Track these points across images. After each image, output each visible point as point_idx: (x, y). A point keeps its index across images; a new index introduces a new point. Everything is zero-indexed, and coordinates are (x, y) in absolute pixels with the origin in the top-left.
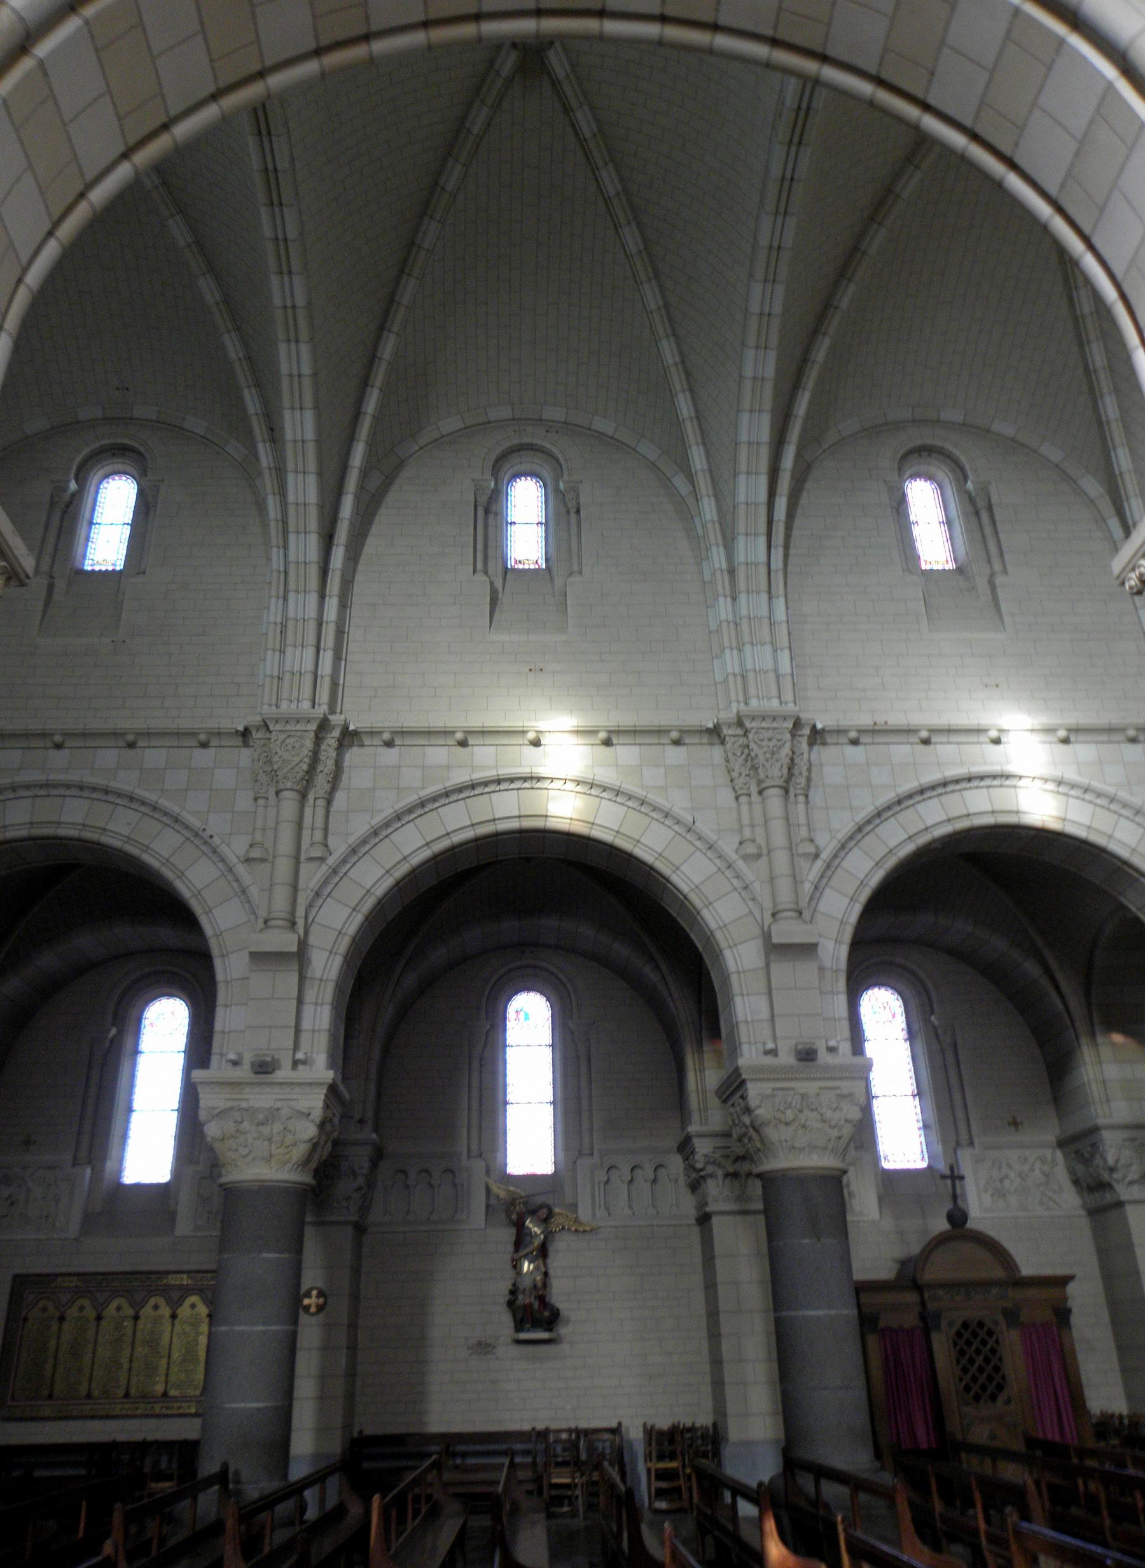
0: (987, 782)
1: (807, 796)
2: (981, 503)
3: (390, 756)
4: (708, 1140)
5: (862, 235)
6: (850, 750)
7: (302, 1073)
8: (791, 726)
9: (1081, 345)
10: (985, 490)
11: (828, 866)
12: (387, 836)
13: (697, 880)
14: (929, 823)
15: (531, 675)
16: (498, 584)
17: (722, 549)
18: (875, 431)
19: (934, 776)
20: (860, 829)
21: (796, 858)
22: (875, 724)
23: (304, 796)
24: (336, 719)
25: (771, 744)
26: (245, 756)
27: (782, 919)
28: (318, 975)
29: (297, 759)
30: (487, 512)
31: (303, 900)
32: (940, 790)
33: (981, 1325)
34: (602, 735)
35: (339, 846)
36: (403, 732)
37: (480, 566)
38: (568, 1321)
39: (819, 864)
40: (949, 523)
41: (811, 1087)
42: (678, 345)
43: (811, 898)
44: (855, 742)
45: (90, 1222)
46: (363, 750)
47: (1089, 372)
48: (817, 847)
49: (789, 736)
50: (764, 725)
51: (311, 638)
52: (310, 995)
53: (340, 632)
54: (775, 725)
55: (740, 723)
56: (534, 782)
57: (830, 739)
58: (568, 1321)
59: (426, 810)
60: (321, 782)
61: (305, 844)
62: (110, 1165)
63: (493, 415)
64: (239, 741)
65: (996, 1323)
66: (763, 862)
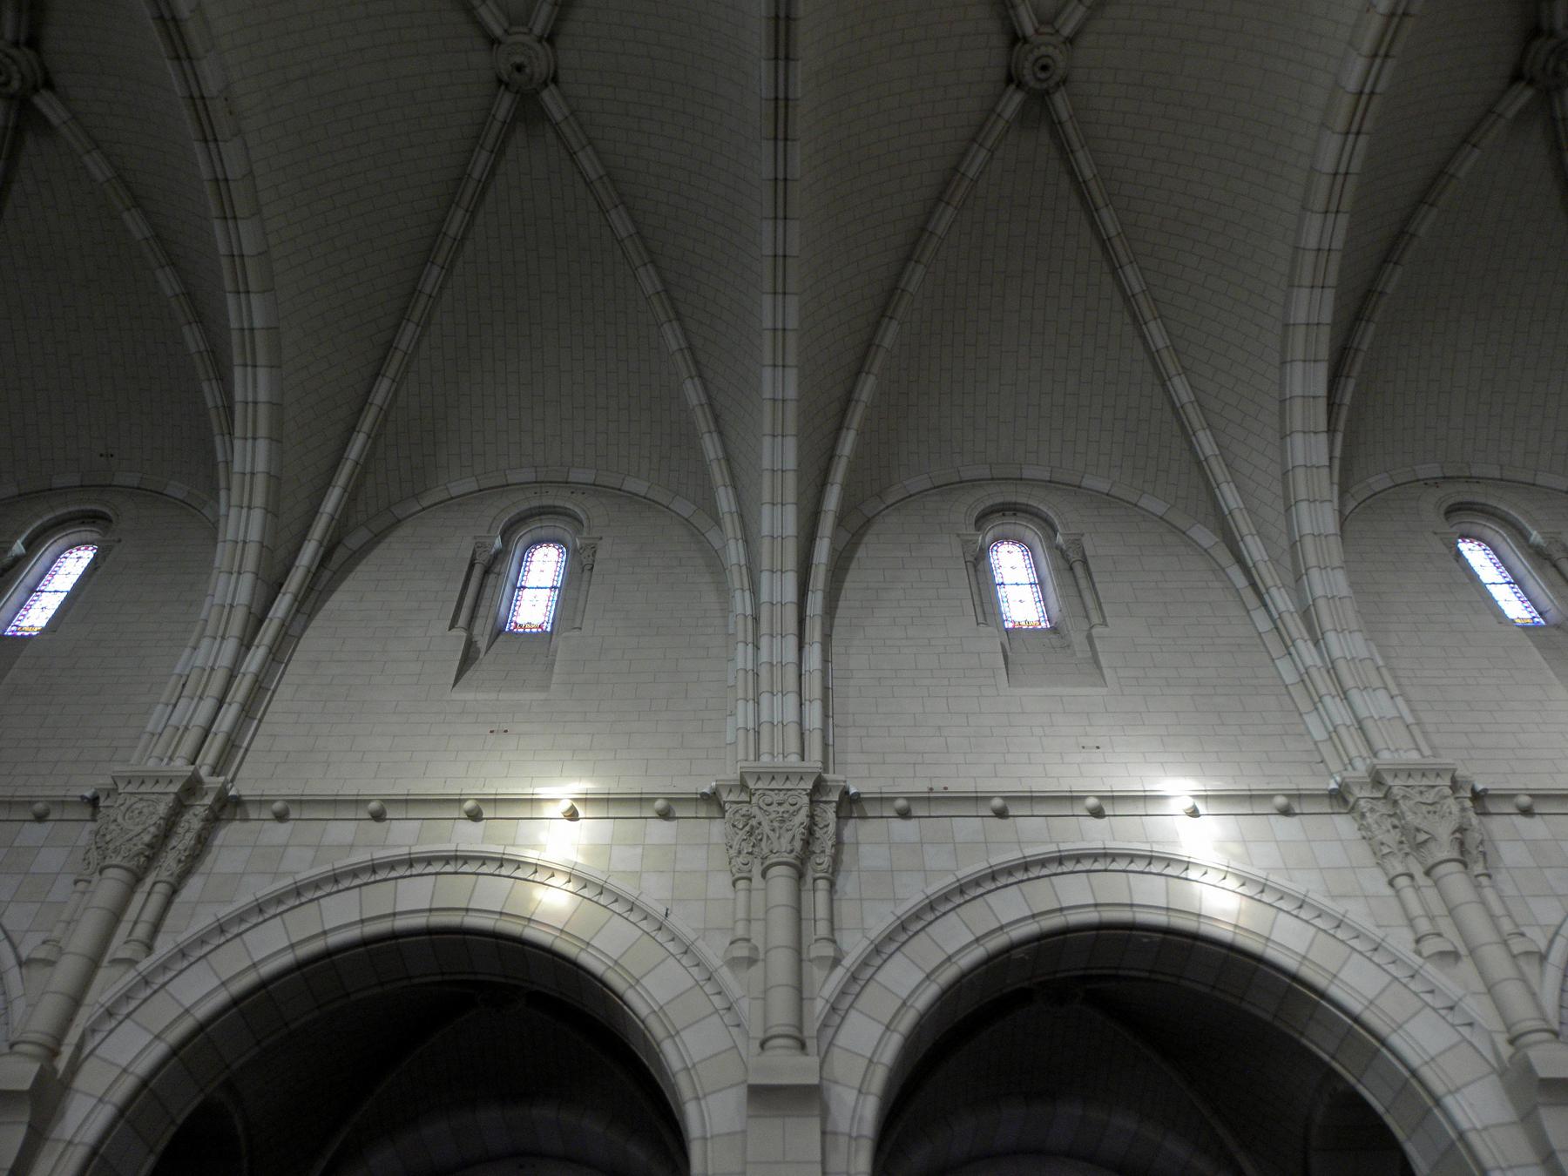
0: (1086, 865)
1: (832, 884)
2: (1073, 556)
3: (281, 831)
5: (900, 275)
6: (899, 825)
8: (810, 786)
9: (1163, 385)
10: (1077, 542)
11: (854, 978)
12: (239, 935)
13: (662, 996)
14: (1004, 922)
15: (493, 737)
16: (482, 643)
17: (747, 594)
18: (948, 488)
20: (903, 927)
21: (806, 965)
22: (931, 789)
23: (137, 878)
25: (781, 809)
26: (83, 834)
27: (774, 1048)
28: (68, 1137)
29: (139, 829)
30: (487, 572)
31: (82, 1019)
32: (1020, 876)
36: (301, 802)
37: (462, 621)
39: (839, 973)
40: (1041, 583)
42: (705, 388)
43: (824, 1025)
44: (904, 814)
46: (246, 825)
47: (1176, 411)
48: (838, 950)
49: (806, 799)
50: (774, 785)
51: (215, 688)
53: (260, 688)
54: (788, 785)
55: (743, 787)
56: (460, 863)
59: (303, 900)
60: (170, 862)
61: (117, 941)
63: (513, 478)
64: (86, 812)
66: (756, 971)
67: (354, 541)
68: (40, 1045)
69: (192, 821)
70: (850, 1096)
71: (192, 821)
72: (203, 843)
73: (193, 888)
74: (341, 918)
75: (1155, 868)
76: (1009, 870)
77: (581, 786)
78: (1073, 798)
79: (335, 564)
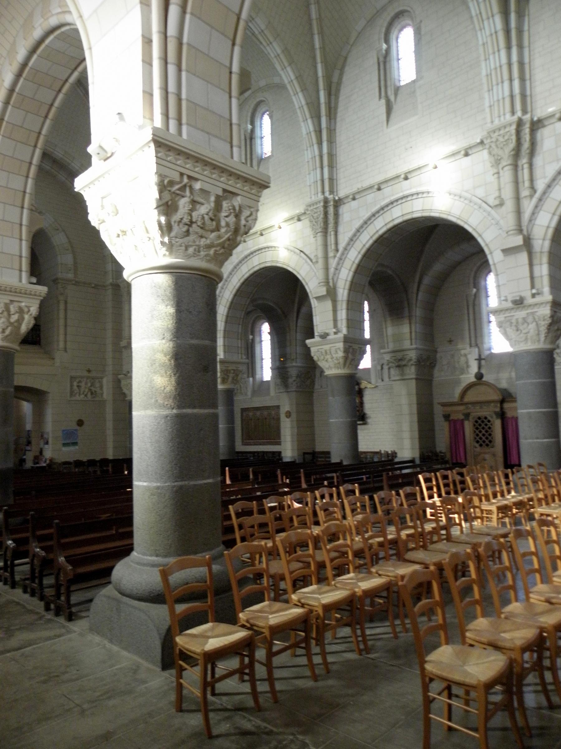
0: (400, 202)
3: (354, 204)
4: (388, 354)
7: (538, 299)
19: (248, 252)
24: (527, 117)
32: (382, 212)
33: (486, 418)
34: (463, 152)
35: (540, 185)
38: (370, 417)
41: (327, 347)
44: (354, 199)
45: (254, 392)
52: (339, 307)
57: (546, 123)
58: (370, 417)
62: (486, 346)
65: (492, 417)
67: (335, 79)
68: (513, 230)
69: (331, 210)
70: (540, 242)
71: (331, 210)
72: (533, 144)
73: (341, 229)
74: (380, 226)
75: (420, 196)
76: (378, 212)
77: (286, 214)
78: (398, 177)
79: (333, 91)
